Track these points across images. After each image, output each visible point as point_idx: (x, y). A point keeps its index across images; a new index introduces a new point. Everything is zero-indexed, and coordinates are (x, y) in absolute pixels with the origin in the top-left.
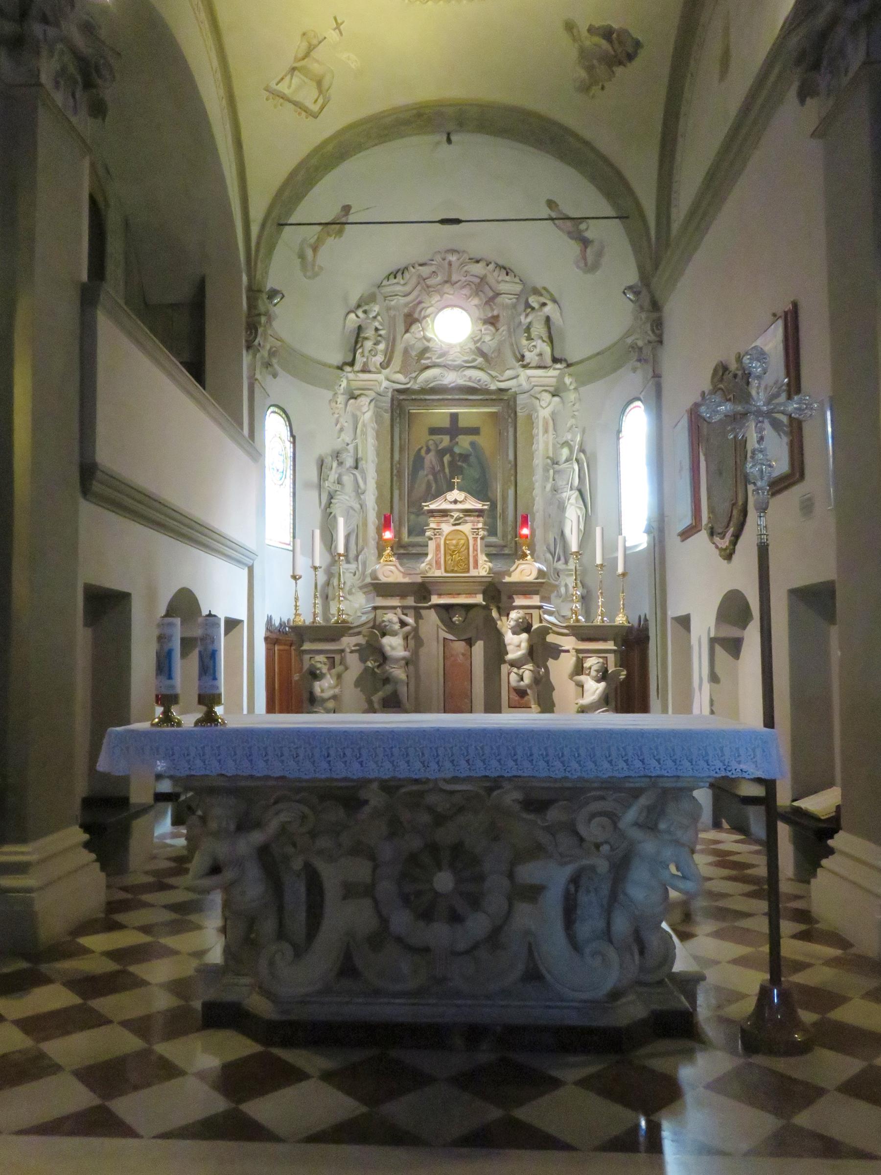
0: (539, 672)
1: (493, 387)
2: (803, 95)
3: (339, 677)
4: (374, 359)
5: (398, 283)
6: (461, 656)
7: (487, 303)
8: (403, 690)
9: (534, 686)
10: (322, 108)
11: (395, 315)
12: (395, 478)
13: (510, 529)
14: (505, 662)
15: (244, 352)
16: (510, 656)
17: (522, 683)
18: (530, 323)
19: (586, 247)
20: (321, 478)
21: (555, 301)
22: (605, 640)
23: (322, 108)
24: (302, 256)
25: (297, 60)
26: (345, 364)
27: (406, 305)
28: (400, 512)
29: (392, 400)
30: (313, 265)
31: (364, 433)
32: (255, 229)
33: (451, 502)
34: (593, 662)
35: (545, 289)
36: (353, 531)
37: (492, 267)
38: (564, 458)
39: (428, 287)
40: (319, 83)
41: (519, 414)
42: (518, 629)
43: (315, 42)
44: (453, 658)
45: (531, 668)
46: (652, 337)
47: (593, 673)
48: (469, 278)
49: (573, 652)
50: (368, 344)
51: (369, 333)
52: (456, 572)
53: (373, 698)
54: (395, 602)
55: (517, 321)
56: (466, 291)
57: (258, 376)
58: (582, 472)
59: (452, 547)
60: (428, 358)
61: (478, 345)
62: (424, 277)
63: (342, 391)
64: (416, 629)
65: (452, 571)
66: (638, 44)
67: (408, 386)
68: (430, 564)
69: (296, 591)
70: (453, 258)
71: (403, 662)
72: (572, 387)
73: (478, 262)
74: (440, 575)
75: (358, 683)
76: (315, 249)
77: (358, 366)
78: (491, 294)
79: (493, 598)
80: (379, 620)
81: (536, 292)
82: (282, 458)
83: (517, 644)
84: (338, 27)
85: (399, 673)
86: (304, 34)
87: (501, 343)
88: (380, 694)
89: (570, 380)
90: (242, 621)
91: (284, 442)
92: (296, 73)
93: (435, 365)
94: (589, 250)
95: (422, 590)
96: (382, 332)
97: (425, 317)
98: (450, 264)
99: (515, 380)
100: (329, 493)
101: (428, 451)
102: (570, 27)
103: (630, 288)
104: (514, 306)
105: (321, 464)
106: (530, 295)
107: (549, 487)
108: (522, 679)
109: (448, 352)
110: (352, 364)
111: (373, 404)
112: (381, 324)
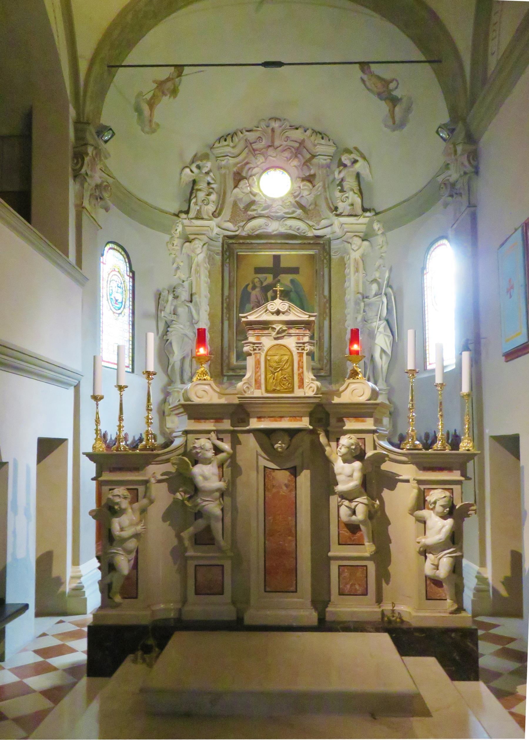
0: (373, 505)
1: (310, 234)
3: (143, 511)
4: (206, 207)
5: (228, 145)
6: (284, 488)
7: (305, 164)
8: (217, 527)
9: (369, 521)
11: (225, 174)
12: (225, 311)
13: (325, 354)
14: (334, 493)
15: (71, 181)
16: (340, 488)
17: (354, 517)
18: (342, 180)
19: (394, 106)
20: (153, 306)
21: (364, 158)
22: (450, 469)
26: (181, 212)
27: (235, 165)
28: (229, 341)
29: (223, 244)
30: (150, 121)
31: (197, 272)
32: (83, 66)
33: (273, 313)
34: (437, 496)
35: (356, 148)
36: (188, 355)
37: (309, 132)
38: (373, 292)
39: (254, 150)
41: (332, 257)
42: (349, 457)
44: (274, 490)
45: (366, 501)
46: (469, 169)
47: (439, 508)
48: (289, 143)
49: (414, 484)
50: (201, 195)
51: (202, 185)
52: (279, 392)
53: (182, 534)
54: (209, 425)
55: (331, 178)
56: (287, 154)
57: (86, 204)
58: (389, 304)
59: (274, 364)
60: (254, 210)
61: (297, 199)
62: (251, 142)
63: (178, 235)
64: (233, 457)
65: (274, 391)
67: (237, 233)
68: (248, 382)
69: (97, 413)
70: (275, 125)
71: (217, 494)
72: (380, 232)
73: (297, 129)
74: (260, 395)
75: (167, 516)
76: (152, 104)
77: (192, 214)
78: (308, 156)
79: (320, 420)
80: (190, 446)
81: (347, 151)
82: (120, 290)
83: (349, 474)
85: (213, 507)
87: (317, 197)
88: (191, 530)
89: (379, 226)
90: (66, 440)
91: (123, 276)
93: (261, 216)
94: (397, 109)
95: (240, 412)
96: (212, 186)
97: (251, 176)
98: (273, 130)
99: (329, 228)
100: (166, 322)
101: (254, 288)
104: (328, 166)
105: (159, 296)
107: (360, 318)
108: (354, 513)
109: (271, 205)
110: (187, 212)
111: (205, 246)
112: (213, 179)
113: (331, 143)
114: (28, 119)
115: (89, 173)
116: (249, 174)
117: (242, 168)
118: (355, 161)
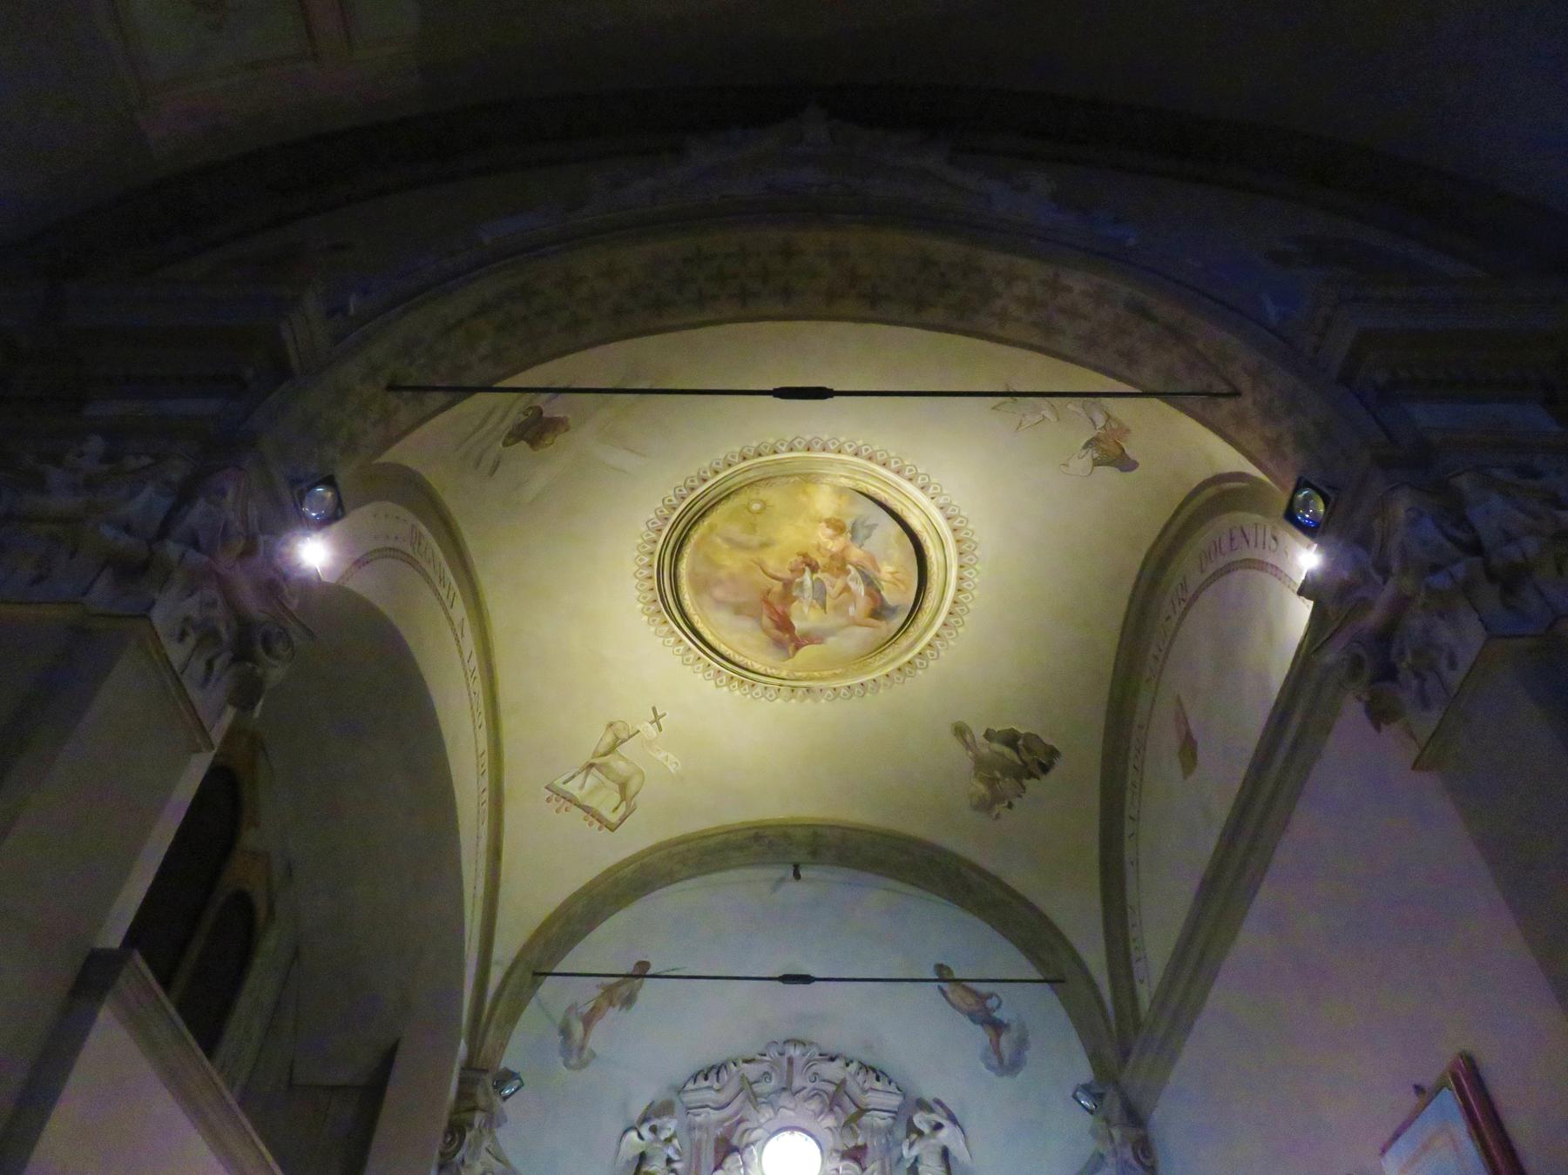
2: (1379, 714)
5: (710, 1088)
10: (622, 820)
11: (700, 1141)
18: (916, 1159)
19: (998, 1036)
21: (953, 1119)
23: (622, 820)
24: (565, 1031)
25: (595, 755)
30: (582, 1048)
35: (939, 1102)
37: (853, 1067)
39: (756, 1096)
40: (623, 787)
43: (624, 735)
48: (818, 1084)
56: (814, 1105)
66: (1053, 753)
70: (794, 1052)
73: (832, 1059)
76: (588, 1021)
78: (853, 1110)
81: (922, 1105)
84: (656, 720)
86: (611, 725)
92: (594, 770)
96: (677, 1166)
97: (747, 1145)
102: (960, 731)
103: (1086, 1088)
104: (890, 1131)
106: (913, 1110)
113: (892, 1088)
114: (388, 1059)
115: (467, 1162)
116: (745, 1140)
117: (731, 1131)
118: (938, 1127)
